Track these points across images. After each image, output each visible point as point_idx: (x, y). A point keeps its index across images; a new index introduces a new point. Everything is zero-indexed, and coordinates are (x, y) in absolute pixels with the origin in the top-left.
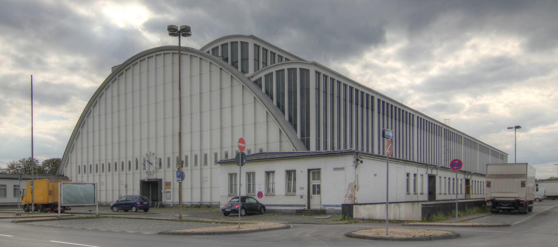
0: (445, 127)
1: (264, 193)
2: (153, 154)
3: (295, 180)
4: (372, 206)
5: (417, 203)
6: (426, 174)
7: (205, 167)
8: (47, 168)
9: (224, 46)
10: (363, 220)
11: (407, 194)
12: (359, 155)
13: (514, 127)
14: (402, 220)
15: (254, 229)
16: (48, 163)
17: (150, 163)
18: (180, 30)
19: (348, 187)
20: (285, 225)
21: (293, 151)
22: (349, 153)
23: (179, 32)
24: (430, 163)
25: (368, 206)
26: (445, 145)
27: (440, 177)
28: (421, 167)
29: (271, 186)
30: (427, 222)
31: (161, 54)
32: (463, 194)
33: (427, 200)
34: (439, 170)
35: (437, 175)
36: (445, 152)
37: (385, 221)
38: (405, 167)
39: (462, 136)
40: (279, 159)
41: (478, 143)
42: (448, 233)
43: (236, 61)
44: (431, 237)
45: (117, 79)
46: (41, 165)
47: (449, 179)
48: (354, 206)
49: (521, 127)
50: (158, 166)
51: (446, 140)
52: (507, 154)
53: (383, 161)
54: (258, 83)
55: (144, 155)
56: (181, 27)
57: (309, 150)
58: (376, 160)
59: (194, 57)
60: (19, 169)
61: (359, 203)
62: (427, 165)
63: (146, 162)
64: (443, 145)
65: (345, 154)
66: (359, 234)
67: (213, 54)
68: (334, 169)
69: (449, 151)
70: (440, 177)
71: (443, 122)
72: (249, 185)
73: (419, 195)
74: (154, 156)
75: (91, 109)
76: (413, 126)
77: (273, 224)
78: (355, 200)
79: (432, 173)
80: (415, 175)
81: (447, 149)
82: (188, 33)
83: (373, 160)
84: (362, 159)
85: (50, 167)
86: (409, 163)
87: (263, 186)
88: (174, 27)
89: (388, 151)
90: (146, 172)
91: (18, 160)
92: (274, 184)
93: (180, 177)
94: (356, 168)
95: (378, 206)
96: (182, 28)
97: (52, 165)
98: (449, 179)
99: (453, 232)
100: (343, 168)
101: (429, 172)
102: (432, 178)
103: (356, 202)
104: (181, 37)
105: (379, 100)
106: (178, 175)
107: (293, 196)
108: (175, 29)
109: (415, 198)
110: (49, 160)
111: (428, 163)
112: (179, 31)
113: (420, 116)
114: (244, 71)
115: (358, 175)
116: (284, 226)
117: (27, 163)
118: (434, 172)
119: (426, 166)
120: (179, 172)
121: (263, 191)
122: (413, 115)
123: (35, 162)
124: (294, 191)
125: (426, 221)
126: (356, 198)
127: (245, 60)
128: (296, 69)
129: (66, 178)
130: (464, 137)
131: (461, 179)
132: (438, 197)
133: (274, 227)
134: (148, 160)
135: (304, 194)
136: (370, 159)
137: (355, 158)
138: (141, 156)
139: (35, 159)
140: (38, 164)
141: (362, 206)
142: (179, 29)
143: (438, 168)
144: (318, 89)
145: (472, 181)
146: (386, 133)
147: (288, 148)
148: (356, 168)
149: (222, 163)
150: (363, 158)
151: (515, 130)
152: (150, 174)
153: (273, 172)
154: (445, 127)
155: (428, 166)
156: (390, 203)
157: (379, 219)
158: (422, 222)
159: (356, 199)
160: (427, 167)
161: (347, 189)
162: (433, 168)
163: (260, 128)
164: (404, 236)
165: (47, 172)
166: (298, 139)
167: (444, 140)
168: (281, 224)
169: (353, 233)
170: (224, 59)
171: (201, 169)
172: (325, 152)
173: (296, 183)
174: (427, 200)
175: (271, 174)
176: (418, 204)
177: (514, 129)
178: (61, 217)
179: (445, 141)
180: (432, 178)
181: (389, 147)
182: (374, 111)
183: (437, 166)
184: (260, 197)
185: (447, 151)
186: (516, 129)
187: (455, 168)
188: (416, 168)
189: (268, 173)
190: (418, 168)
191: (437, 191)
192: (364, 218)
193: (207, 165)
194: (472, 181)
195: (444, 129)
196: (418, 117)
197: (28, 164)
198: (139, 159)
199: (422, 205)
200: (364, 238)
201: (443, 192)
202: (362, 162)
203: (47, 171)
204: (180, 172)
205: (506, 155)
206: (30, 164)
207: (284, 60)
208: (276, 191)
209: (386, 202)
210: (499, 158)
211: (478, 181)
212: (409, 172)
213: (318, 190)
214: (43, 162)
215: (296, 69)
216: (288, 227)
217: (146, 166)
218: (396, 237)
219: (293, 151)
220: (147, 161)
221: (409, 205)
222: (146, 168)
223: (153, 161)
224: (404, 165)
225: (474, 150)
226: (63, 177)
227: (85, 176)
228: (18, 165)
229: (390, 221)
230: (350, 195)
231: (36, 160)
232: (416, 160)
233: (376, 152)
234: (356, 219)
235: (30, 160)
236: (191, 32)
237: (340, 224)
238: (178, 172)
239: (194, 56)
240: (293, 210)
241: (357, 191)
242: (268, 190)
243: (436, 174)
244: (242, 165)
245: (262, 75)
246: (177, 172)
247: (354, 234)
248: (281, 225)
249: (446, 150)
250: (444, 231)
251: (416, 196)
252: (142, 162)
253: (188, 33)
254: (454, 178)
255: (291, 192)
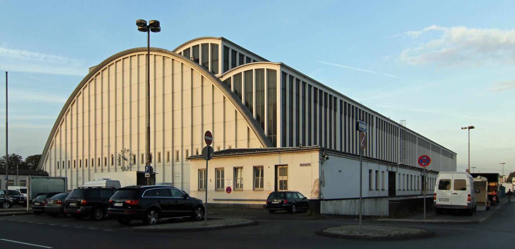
0: (401, 128)
1: (232, 188)
2: (128, 150)
3: (262, 175)
4: (338, 201)
5: (380, 199)
6: (387, 171)
7: (177, 163)
8: (30, 164)
9: (196, 47)
10: (330, 215)
11: (369, 189)
12: (325, 152)
13: (467, 127)
14: (367, 215)
15: (221, 225)
16: (31, 159)
17: (125, 159)
18: (149, 25)
19: (314, 183)
20: (253, 221)
21: (261, 147)
22: (315, 150)
23: (149, 27)
24: (390, 161)
25: (334, 201)
26: (401, 145)
27: (399, 174)
28: (382, 165)
29: (239, 181)
30: (394, 218)
31: (136, 55)
32: (420, 190)
33: (388, 196)
34: (399, 167)
35: (397, 172)
36: (401, 151)
37: (358, 217)
38: (367, 164)
39: (416, 136)
40: (247, 155)
41: (431, 143)
42: (423, 231)
43: (207, 62)
44: (407, 235)
45: (94, 79)
46: (25, 161)
47: (408, 175)
48: (322, 202)
49: (474, 127)
50: (132, 162)
51: (402, 140)
52: (457, 154)
53: (347, 158)
54: (226, 85)
55: (119, 151)
56: (149, 22)
57: (276, 147)
58: (341, 157)
59: (167, 58)
60: (3, 164)
61: (324, 198)
62: (388, 162)
63: (121, 158)
64: (399, 145)
65: (311, 150)
66: (331, 232)
67: (185, 56)
68: (301, 165)
69: (405, 150)
70: (399, 174)
71: (399, 123)
72: (218, 181)
73: (381, 191)
74: (129, 152)
75: (69, 108)
76: (372, 126)
77: (241, 219)
78: (321, 196)
79: (392, 170)
80: (377, 172)
81: (403, 148)
82: (157, 28)
83: (338, 156)
84: (328, 156)
85: (33, 163)
86: (371, 160)
87: (231, 181)
88: (143, 22)
89: (362, 144)
90: (121, 168)
91: (2, 156)
92: (242, 179)
93: (149, 172)
94: (322, 164)
95: (344, 201)
96: (151, 22)
97: (35, 161)
98: (411, 176)
99: (427, 230)
100: (309, 165)
101: (390, 169)
102: (392, 175)
103: (322, 197)
104: (151, 32)
105: (341, 101)
106: (147, 169)
107: (260, 192)
108: (143, 23)
109: (376, 194)
110: (32, 156)
111: (388, 160)
112: (148, 26)
113: (379, 117)
114: (213, 72)
115: (324, 171)
116: (252, 222)
117: (10, 159)
118: (394, 169)
119: (387, 163)
120: (147, 167)
121: (232, 186)
122: (372, 116)
123: (18, 158)
124: (262, 186)
125: (394, 217)
126: (322, 193)
127: (215, 61)
128: (264, 69)
129: (46, 174)
130: (418, 138)
131: (418, 176)
132: (398, 193)
133: (242, 223)
134: (123, 156)
135: (271, 189)
136: (335, 156)
137: (321, 154)
138: (116, 153)
139: (19, 155)
140: (21, 160)
141: (329, 202)
142: (148, 24)
143: (397, 165)
144: (284, 89)
145: (428, 178)
146: (360, 125)
147: (257, 143)
148: (322, 164)
149: (192, 158)
150: (329, 155)
151: (469, 130)
152: (125, 170)
153: (242, 168)
154: (401, 128)
155: (389, 163)
156: (363, 198)
157: (345, 214)
158: (390, 217)
159: (322, 194)
160: (388, 164)
161: (313, 184)
162: (393, 165)
163: (230, 126)
164: (378, 235)
165: (31, 168)
166: (266, 136)
167: (400, 139)
168: (249, 220)
169: (324, 231)
170: (195, 60)
171: (173, 165)
172: (292, 149)
173: (263, 178)
174: (388, 196)
175: (239, 170)
176: (381, 199)
177: (468, 129)
178: (30, 212)
179: (401, 140)
180: (392, 175)
181: (363, 141)
182: (337, 112)
183: (397, 163)
184: (228, 192)
185: (403, 150)
186: (470, 129)
187: (423, 164)
188: (378, 165)
189: (236, 170)
190: (380, 165)
191: (397, 188)
192: (331, 214)
193: (179, 161)
194: (428, 178)
195: (401, 129)
196: (377, 118)
197: (12, 160)
198: (114, 155)
199: (390, 201)
200: (337, 236)
201: (402, 188)
202: (327, 158)
203: (30, 166)
204: (148, 167)
205: (455, 154)
206: (13, 160)
207: (252, 60)
208: (244, 186)
209: (359, 196)
210: (449, 157)
211: (433, 178)
212: (371, 169)
213: (285, 185)
214: (26, 158)
215: (264, 69)
216: (255, 224)
217: (121, 162)
218: (370, 235)
219: (261, 147)
220: (122, 157)
221: (373, 202)
222: (122, 164)
223: (127, 155)
224: (367, 162)
225: (425, 149)
226: (42, 172)
227: (63, 171)
228: (2, 161)
229: (365, 217)
230: (316, 191)
231: (20, 156)
232: (374, 157)
233: (338, 149)
234: (323, 214)
235: (13, 156)
236: (160, 27)
237: (307, 219)
238: (147, 167)
239: (166, 57)
240: (260, 205)
241: (323, 186)
242: (236, 185)
243: (395, 171)
244: (209, 159)
245: (231, 75)
246: (146, 167)
247: (326, 233)
248: (249, 221)
249: (402, 149)
250: (418, 228)
251: (378, 192)
252: (118, 158)
253: (157, 28)
254: (418, 175)
255: (259, 188)
